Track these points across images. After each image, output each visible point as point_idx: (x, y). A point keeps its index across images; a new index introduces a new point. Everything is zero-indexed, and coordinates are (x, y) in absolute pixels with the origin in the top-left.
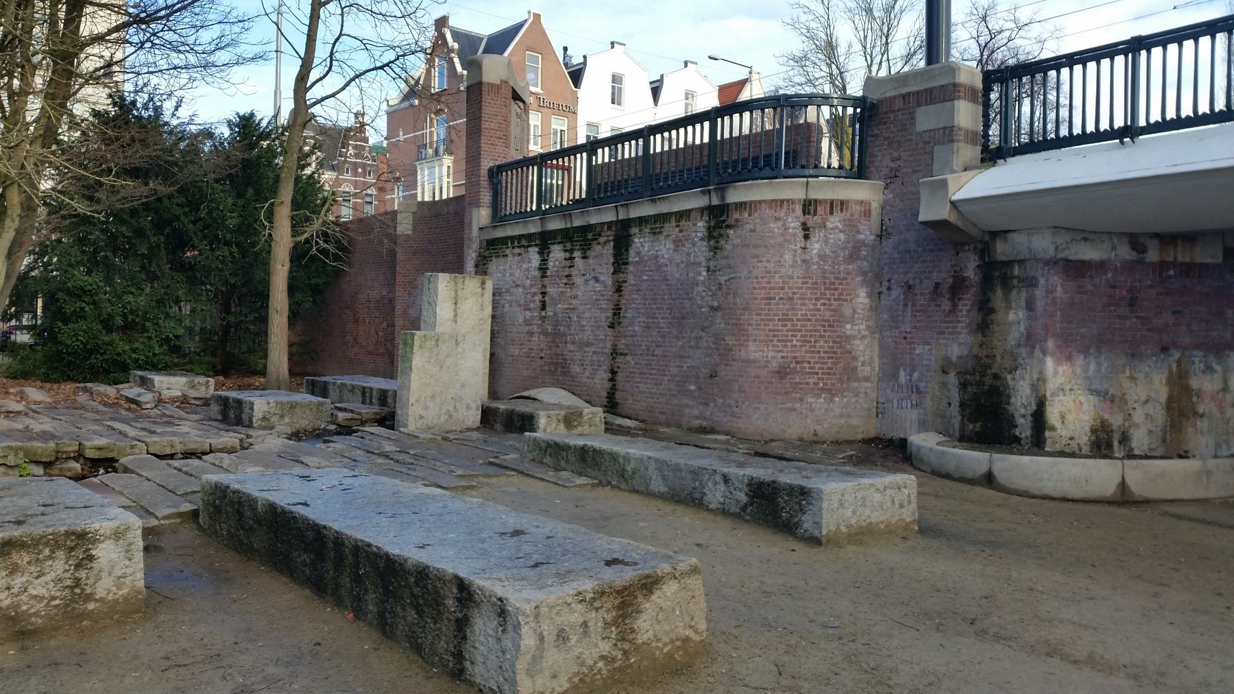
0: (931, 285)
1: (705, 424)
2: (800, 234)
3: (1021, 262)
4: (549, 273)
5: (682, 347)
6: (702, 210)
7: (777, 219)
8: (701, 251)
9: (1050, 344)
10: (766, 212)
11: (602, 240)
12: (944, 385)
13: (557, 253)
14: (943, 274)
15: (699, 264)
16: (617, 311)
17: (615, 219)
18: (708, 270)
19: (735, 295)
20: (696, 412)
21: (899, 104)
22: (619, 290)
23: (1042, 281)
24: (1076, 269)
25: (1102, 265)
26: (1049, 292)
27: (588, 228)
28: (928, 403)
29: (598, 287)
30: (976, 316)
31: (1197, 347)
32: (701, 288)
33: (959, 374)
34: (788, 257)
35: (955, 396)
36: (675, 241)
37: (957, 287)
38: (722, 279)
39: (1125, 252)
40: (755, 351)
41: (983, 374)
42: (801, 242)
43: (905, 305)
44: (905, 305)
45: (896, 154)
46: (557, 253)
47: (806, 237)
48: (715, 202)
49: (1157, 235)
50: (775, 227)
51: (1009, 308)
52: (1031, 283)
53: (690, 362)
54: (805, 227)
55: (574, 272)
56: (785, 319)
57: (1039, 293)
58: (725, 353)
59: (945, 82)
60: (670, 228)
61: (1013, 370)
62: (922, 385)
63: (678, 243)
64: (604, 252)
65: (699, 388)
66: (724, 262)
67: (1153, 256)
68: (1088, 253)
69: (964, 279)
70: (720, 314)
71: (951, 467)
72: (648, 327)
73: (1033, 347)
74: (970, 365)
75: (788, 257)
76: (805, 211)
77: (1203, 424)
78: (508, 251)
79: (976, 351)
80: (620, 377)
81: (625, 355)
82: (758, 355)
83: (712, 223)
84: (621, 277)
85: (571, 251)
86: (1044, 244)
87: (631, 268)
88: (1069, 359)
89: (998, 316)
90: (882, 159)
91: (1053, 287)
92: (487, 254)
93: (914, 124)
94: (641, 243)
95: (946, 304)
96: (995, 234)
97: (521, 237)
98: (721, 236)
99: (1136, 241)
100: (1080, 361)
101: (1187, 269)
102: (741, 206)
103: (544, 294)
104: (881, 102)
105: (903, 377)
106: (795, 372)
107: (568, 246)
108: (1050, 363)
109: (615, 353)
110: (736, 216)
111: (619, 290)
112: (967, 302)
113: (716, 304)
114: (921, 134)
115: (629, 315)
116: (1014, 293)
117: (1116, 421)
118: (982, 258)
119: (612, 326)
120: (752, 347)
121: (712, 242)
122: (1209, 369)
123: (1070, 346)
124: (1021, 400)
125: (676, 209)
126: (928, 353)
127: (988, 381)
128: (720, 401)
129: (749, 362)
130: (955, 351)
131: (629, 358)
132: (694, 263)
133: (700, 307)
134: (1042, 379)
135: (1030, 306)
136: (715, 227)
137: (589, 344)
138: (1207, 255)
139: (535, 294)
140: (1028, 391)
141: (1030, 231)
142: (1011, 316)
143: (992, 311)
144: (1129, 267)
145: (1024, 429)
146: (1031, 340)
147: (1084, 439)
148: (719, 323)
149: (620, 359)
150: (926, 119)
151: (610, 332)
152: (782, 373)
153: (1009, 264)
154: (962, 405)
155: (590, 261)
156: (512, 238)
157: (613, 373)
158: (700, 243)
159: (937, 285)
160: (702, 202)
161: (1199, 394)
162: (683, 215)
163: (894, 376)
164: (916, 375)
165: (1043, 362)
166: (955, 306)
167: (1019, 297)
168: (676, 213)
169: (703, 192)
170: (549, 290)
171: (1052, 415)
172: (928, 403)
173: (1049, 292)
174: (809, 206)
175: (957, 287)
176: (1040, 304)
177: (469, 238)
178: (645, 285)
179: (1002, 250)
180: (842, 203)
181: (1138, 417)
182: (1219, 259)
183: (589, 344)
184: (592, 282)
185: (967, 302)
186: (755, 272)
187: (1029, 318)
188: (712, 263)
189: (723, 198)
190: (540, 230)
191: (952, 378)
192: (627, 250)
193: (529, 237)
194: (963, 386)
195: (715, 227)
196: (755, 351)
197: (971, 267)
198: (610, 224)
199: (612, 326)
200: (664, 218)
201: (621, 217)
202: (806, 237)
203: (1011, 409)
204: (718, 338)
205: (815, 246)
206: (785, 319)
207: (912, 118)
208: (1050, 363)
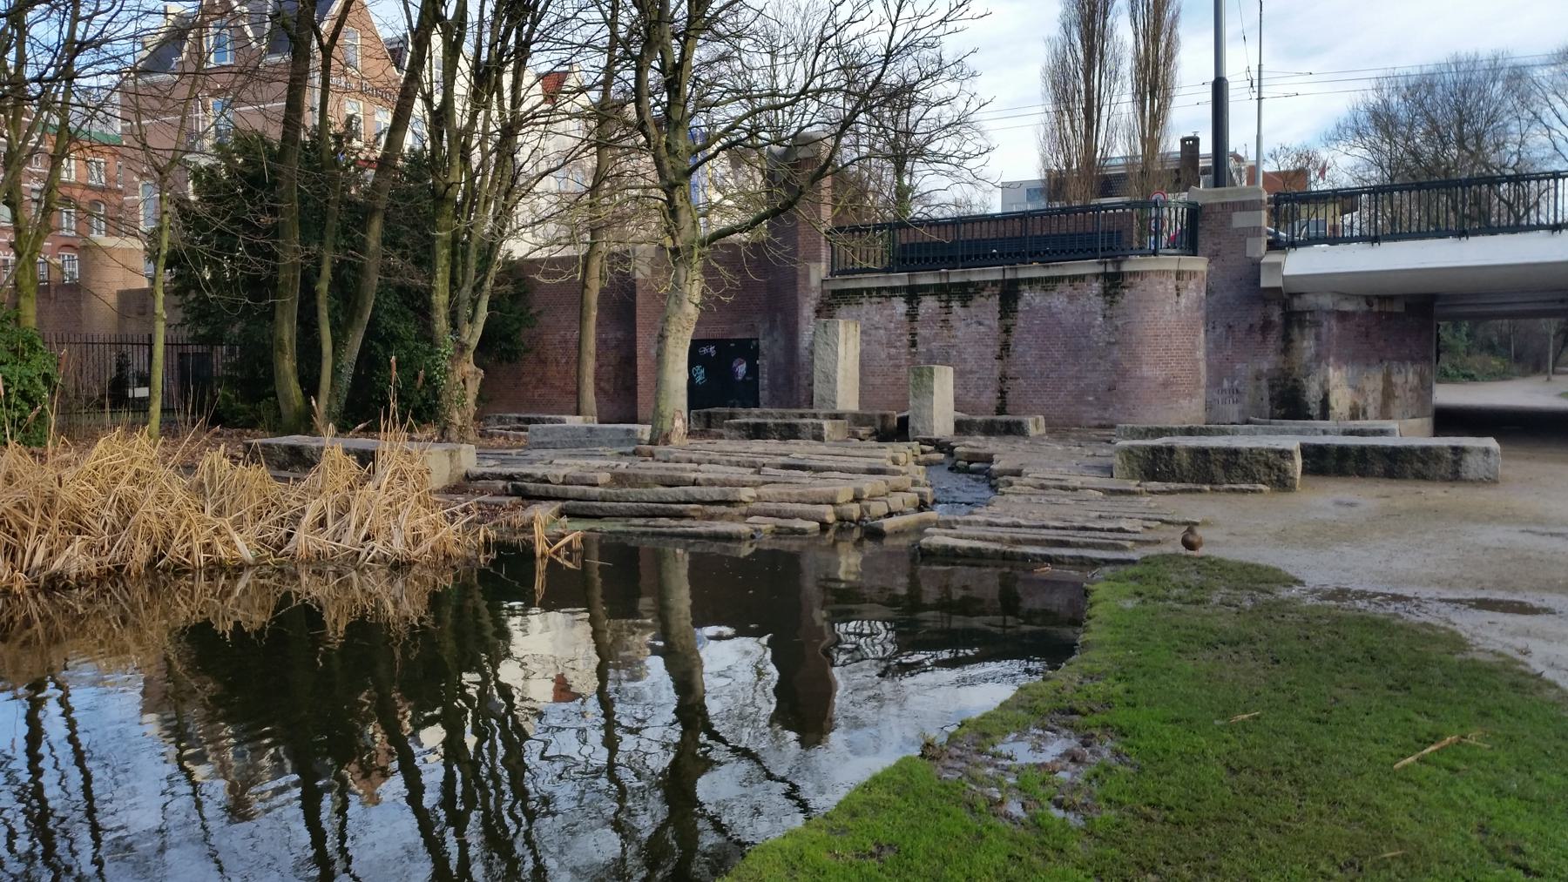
0: (1247, 326)
1: (1104, 422)
2: (1175, 293)
3: (1311, 312)
4: (919, 318)
5: (1080, 371)
6: (1097, 276)
7: (1161, 283)
8: (1098, 304)
9: (1331, 359)
10: (1152, 276)
11: (985, 293)
12: (1258, 388)
13: (929, 304)
14: (1256, 317)
15: (1096, 313)
16: (1005, 347)
17: (1000, 278)
18: (1104, 317)
19: (1130, 334)
20: (1095, 415)
21: (1218, 209)
22: (1007, 331)
23: (1326, 323)
24: (1343, 316)
25: (1354, 313)
26: (1330, 329)
27: (970, 284)
28: (1246, 399)
29: (982, 329)
30: (1281, 344)
31: (1394, 359)
32: (1097, 330)
33: (1269, 380)
34: (1168, 308)
35: (1266, 394)
36: (1068, 297)
37: (1266, 326)
38: (1119, 323)
39: (1364, 307)
40: (1147, 371)
41: (1286, 379)
42: (1175, 298)
43: (1227, 338)
44: (1227, 338)
45: (1217, 241)
46: (929, 304)
47: (1178, 295)
48: (1110, 269)
49: (1377, 297)
50: (1160, 288)
51: (1303, 338)
52: (1318, 324)
53: (1087, 381)
54: (1177, 289)
55: (951, 317)
56: (1167, 349)
57: (1324, 330)
58: (1124, 375)
59: (1254, 198)
60: (1065, 287)
61: (1306, 376)
62: (1241, 389)
63: (1071, 298)
64: (987, 308)
65: (1097, 399)
66: (1120, 311)
67: (1376, 308)
68: (1348, 307)
69: (1271, 322)
70: (1117, 347)
71: (578, 511)
72: (1041, 358)
73: (1320, 362)
74: (1277, 374)
75: (1168, 308)
76: (1177, 279)
77: (1397, 402)
78: (863, 300)
79: (1281, 365)
80: (1010, 396)
81: (1016, 379)
82: (1150, 373)
83: (1108, 285)
84: (1009, 322)
85: (949, 301)
86: (1327, 302)
87: (1021, 315)
88: (1340, 368)
89: (1296, 344)
90: (1204, 241)
91: (1332, 327)
92: (833, 301)
93: (1230, 223)
94: (1029, 297)
95: (1259, 338)
96: (1292, 295)
97: (879, 290)
98: (1116, 293)
99: (1368, 299)
100: (1344, 368)
101: (1391, 316)
102: (1134, 274)
103: (914, 335)
104: (1204, 206)
105: (1226, 384)
106: (1172, 383)
107: (944, 297)
108: (1331, 370)
109: (1003, 378)
110: (1131, 280)
111: (1007, 331)
112: (1274, 337)
113: (1113, 340)
114: (1237, 230)
115: (1020, 349)
116: (1307, 330)
117: (1360, 402)
118: (1284, 308)
119: (1000, 358)
120: (1145, 368)
121: (1108, 298)
122: (1400, 372)
123: (1342, 360)
124: (1313, 392)
125: (1069, 273)
126: (1246, 369)
127: (1290, 383)
128: (1118, 406)
129: (1142, 378)
130: (1265, 366)
131: (1021, 381)
132: (1090, 312)
133: (1097, 343)
134: (1327, 380)
135: (1318, 337)
136: (1110, 288)
137: (971, 372)
138: (1398, 308)
139: (902, 334)
140: (1317, 387)
141: (1316, 293)
142: (1305, 344)
143: (1292, 341)
144: (1369, 313)
145: (1315, 409)
146: (1319, 358)
147: (1347, 413)
148: (1116, 353)
149: (1009, 382)
150: (1240, 220)
151: (997, 362)
152: (1166, 385)
153: (1303, 313)
154: (1272, 399)
155: (972, 309)
156: (869, 291)
157: (1003, 393)
158: (1095, 299)
159: (1251, 326)
160: (1100, 269)
161: (1396, 385)
162: (1082, 278)
163: (1220, 384)
164: (1236, 383)
165: (1326, 370)
166: (1265, 338)
167: (1310, 333)
168: (1069, 277)
169: (1099, 263)
170: (919, 331)
171: (1333, 401)
172: (1246, 399)
173: (1330, 329)
174: (1179, 275)
175: (1266, 326)
176: (1324, 337)
177: (806, 288)
178: (1036, 328)
179: (1297, 304)
180: (1195, 273)
181: (1370, 400)
182: (1403, 310)
183: (971, 372)
184: (974, 325)
185: (1274, 337)
186: (1146, 319)
187: (1318, 345)
188: (1108, 312)
189: (1119, 268)
190: (907, 283)
191: (1264, 383)
192: (1016, 302)
193: (893, 291)
194: (1272, 387)
195: (1110, 288)
196: (1147, 371)
197: (1276, 315)
198: (995, 283)
199: (1000, 358)
200: (1060, 279)
201: (1007, 277)
202: (1178, 295)
203: (1306, 399)
204: (1116, 364)
205: (1183, 301)
206: (1167, 349)
207: (1230, 218)
208: (1331, 370)
